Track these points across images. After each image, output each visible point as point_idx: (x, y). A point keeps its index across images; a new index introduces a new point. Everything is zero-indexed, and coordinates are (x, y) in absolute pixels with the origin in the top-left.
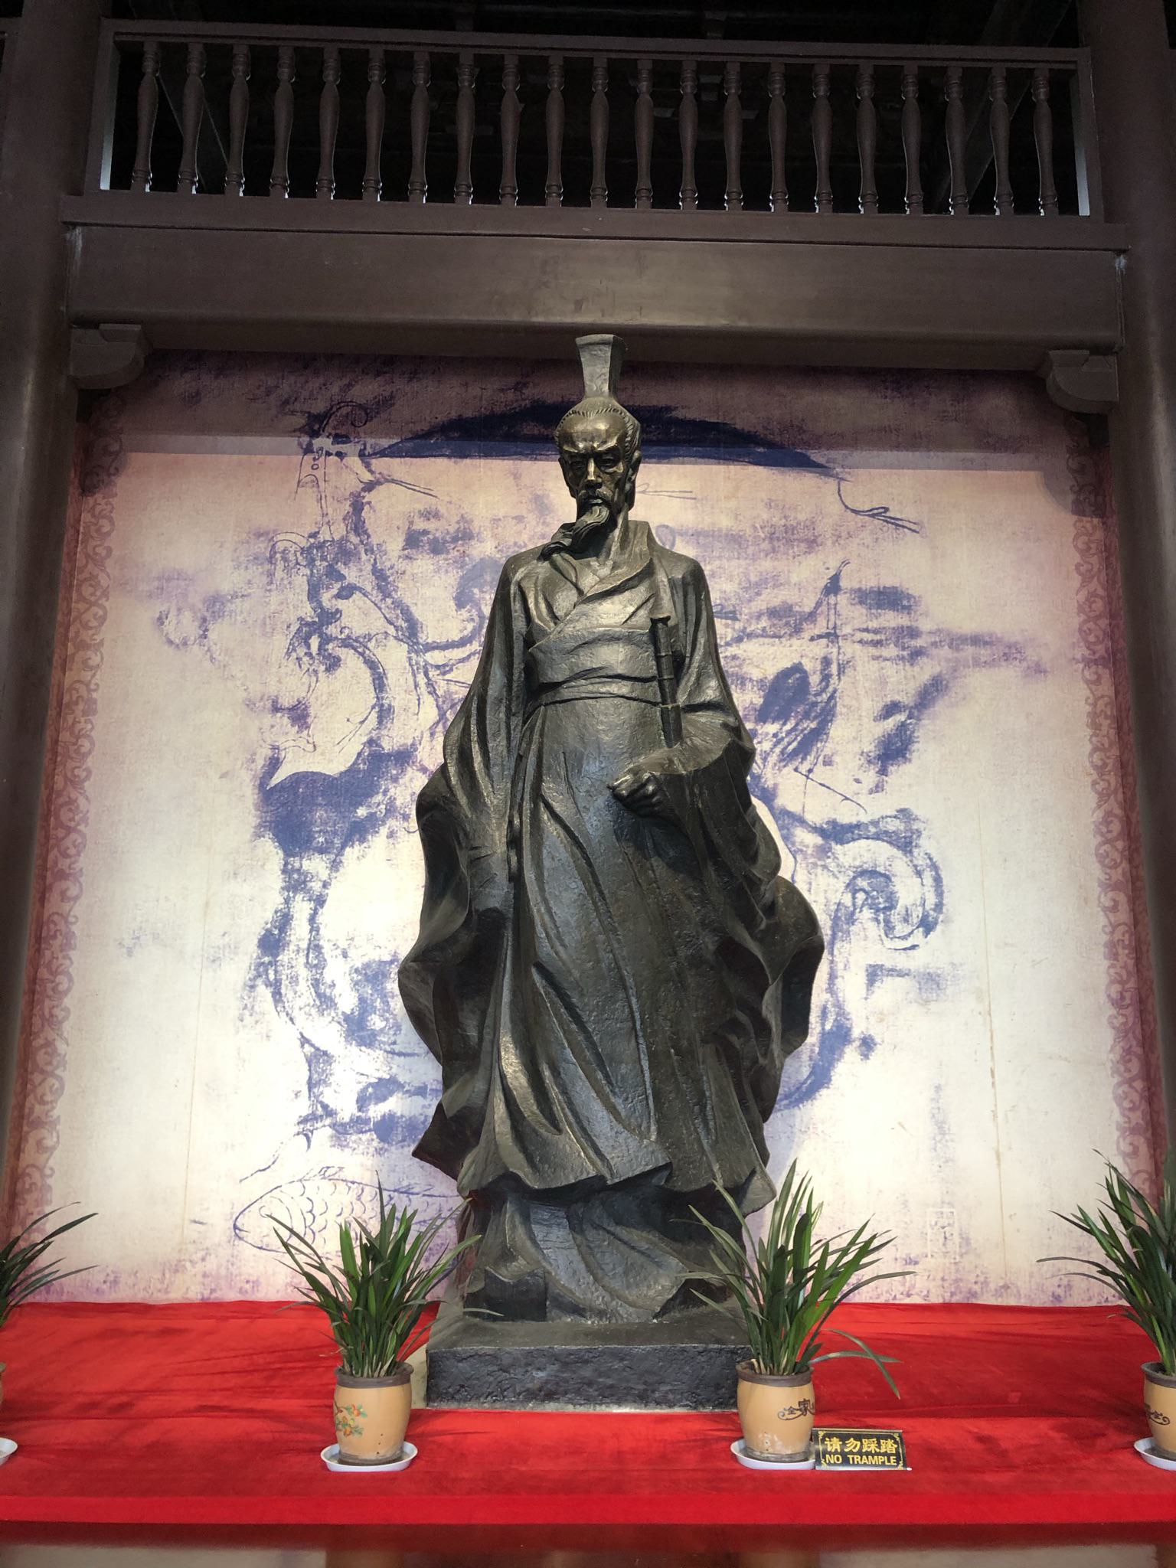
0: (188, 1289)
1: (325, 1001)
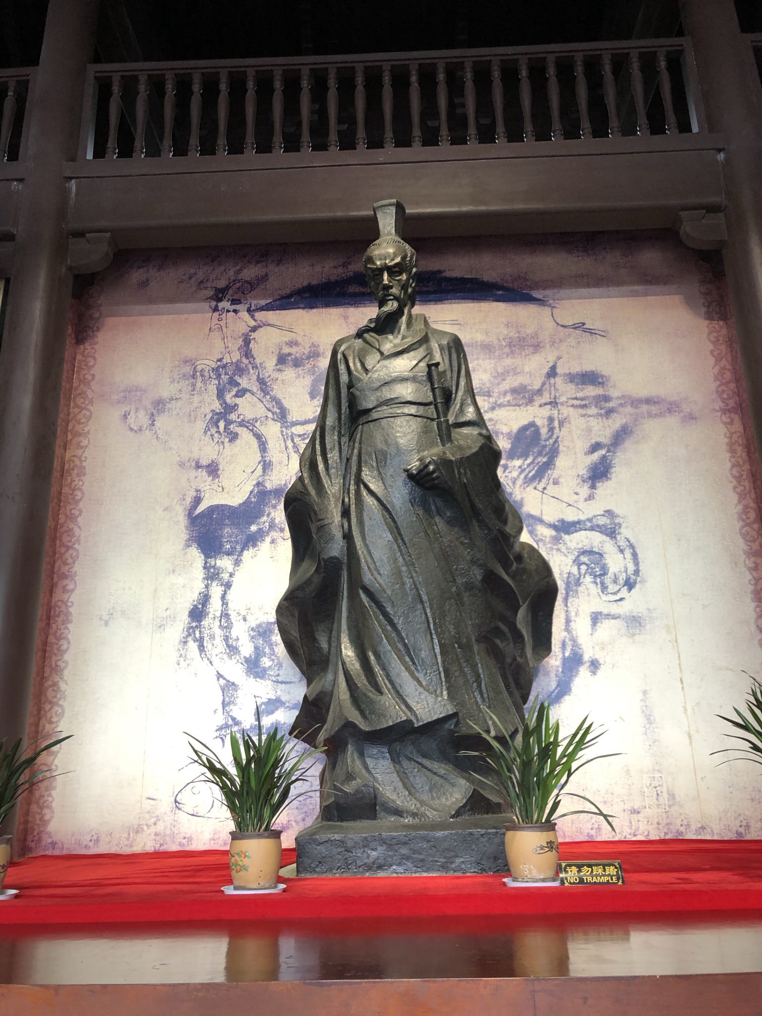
0: (145, 843)
1: (232, 649)
